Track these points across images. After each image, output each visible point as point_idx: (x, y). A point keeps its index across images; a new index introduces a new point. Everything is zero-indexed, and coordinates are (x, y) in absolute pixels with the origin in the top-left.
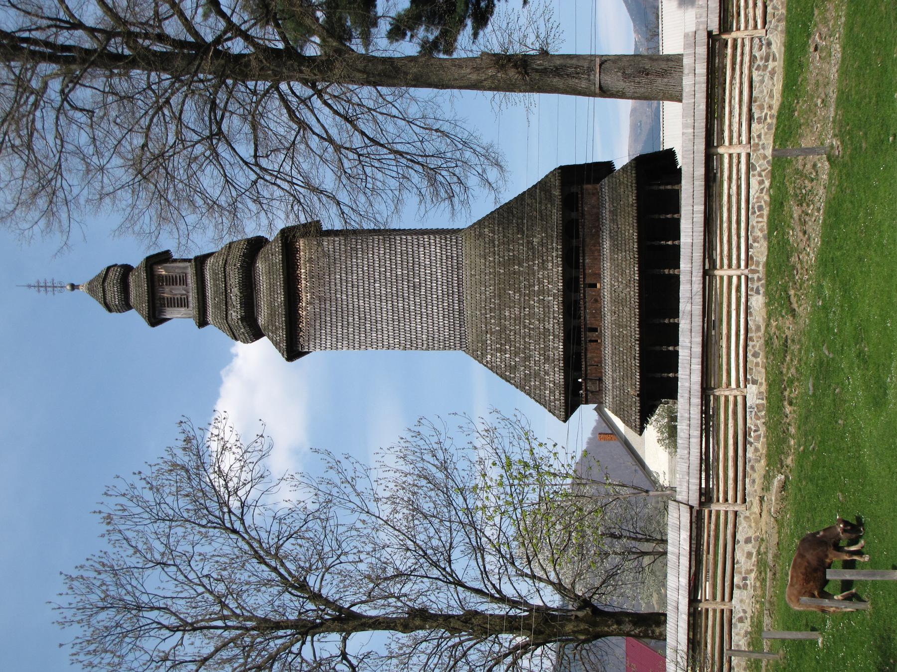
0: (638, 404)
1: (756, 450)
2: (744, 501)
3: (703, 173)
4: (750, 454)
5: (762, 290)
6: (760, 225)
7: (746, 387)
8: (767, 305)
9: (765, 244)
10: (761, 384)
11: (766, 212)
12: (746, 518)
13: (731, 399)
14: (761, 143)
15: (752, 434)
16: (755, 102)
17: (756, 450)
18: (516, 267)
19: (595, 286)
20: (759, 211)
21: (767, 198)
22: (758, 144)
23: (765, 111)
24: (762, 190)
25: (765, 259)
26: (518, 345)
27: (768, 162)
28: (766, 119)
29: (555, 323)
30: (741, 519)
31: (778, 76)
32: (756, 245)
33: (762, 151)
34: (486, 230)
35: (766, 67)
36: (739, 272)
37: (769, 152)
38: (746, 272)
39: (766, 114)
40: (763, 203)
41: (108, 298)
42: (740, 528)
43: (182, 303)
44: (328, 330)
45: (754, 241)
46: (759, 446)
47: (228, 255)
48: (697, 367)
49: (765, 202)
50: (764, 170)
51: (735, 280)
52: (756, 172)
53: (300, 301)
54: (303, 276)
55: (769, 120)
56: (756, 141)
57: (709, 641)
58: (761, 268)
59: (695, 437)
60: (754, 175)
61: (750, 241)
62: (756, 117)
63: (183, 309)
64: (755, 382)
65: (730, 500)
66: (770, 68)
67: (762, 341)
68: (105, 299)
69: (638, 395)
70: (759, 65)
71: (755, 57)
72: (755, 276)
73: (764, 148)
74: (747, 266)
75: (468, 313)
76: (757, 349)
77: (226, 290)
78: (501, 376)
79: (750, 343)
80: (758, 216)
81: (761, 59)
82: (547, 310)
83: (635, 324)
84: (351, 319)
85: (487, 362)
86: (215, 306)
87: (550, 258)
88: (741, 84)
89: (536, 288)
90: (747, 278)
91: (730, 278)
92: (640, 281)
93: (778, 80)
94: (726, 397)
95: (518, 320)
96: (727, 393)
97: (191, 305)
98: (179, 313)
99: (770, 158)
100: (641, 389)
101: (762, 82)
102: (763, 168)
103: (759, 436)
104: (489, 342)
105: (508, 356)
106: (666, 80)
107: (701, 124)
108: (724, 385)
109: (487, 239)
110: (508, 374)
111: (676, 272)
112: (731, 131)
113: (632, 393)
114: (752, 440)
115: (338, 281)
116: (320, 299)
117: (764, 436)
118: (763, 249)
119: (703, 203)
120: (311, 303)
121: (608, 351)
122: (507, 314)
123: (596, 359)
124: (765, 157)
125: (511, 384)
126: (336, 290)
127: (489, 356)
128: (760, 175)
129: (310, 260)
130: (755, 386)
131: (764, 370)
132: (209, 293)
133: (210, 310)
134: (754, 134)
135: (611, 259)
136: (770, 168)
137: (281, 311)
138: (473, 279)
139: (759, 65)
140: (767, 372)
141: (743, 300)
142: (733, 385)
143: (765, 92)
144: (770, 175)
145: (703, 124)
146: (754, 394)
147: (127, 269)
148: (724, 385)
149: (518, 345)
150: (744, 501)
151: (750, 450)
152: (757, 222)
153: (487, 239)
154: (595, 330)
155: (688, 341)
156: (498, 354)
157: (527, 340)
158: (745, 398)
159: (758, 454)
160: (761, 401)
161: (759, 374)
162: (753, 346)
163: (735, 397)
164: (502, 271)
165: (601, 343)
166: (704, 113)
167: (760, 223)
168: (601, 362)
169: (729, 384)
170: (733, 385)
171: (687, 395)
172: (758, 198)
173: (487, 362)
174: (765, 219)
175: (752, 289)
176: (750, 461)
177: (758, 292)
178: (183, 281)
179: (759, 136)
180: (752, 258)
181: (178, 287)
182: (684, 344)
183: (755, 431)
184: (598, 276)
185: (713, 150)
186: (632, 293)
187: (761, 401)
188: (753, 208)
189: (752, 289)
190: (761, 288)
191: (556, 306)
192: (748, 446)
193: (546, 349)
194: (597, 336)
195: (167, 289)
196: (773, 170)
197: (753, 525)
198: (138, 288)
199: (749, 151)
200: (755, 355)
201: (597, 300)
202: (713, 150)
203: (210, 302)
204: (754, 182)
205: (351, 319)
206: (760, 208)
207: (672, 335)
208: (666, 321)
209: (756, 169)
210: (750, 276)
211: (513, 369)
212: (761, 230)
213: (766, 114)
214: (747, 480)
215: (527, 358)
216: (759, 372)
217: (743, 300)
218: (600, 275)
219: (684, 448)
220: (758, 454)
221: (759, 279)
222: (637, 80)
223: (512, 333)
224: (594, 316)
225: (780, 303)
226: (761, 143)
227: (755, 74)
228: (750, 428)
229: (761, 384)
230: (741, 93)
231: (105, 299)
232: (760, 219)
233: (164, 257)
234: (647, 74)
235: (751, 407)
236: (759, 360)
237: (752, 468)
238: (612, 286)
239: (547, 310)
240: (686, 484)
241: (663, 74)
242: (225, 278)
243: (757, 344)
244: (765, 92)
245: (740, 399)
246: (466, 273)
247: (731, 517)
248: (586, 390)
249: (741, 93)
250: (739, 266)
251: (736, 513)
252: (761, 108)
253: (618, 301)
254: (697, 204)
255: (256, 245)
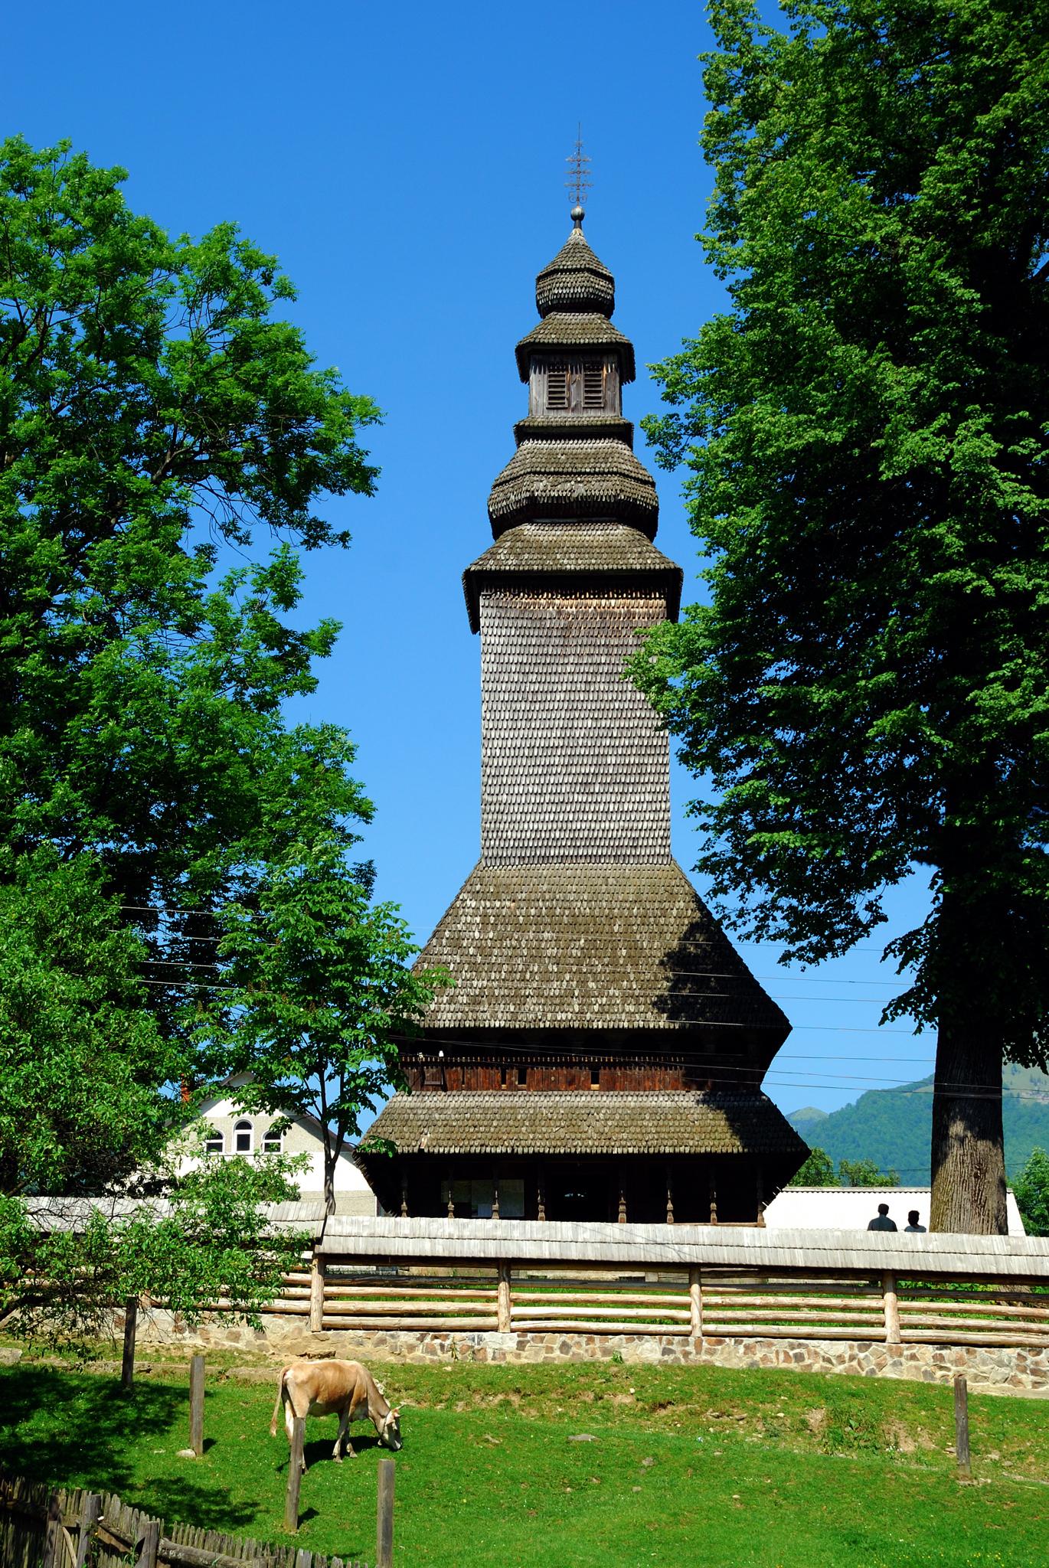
0: (406, 1150)
1: (412, 1348)
2: (326, 1328)
3: (856, 1266)
4: (406, 1337)
5: (669, 1358)
6: (773, 1356)
7: (513, 1331)
8: (649, 1368)
9: (743, 1365)
10: (518, 1356)
11: (792, 1365)
12: (300, 1330)
13: (683, 1314)
14: (903, 1359)
15: (438, 1341)
16: (968, 1352)
17: (412, 1348)
18: (624, 952)
19: (595, 1081)
20: (795, 1355)
21: (816, 1368)
22: (901, 1355)
23: (954, 1368)
24: (829, 1361)
25: (718, 1364)
26: (496, 952)
27: (873, 1371)
28: (941, 1368)
29: (534, 1014)
30: (296, 1322)
31: (1009, 1390)
32: (741, 1349)
33: (890, 1361)
34: (682, 904)
35: (1024, 1371)
36: (696, 1321)
37: (889, 1373)
38: (697, 1333)
39: (948, 1369)
40: (807, 1362)
41: (564, 277)
42: (281, 1321)
43: (556, 400)
44: (515, 640)
45: (747, 1347)
46: (418, 1353)
47: (637, 479)
48: (546, 1252)
49: (810, 1366)
50: (859, 1364)
51: (683, 1314)
52: (856, 1351)
53: (564, 595)
54: (603, 602)
55: (939, 1373)
56: (906, 1353)
57: (728, 1300)
58: (705, 1357)
59: (433, 1246)
60: (851, 1347)
61: (746, 1341)
62: (944, 1352)
63: (545, 400)
64: (521, 1345)
65: (329, 1304)
66: (1023, 1377)
67: (587, 1358)
68: (563, 271)
69: (421, 1151)
70: (1025, 1358)
71: (1038, 1354)
72: (691, 1348)
73: (894, 1364)
74: (706, 1334)
75: (544, 870)
76: (574, 1349)
77: (580, 474)
78: (441, 923)
79: (584, 1338)
80: (786, 1353)
81: (1037, 1363)
82: (558, 1001)
83: (542, 1146)
84: (534, 677)
85: (463, 901)
86: (552, 454)
87: (642, 1008)
88: (991, 1329)
89: (591, 985)
90: (687, 1334)
91: (687, 1306)
92: (609, 1156)
93: (1003, 1390)
94: (495, 1299)
95: (536, 956)
96: (503, 1299)
97: (552, 414)
98: (538, 393)
99: (879, 1375)
100: (431, 1155)
101: (1000, 1364)
102: (864, 1363)
103: (433, 1352)
104: (498, 904)
105: (477, 935)
106: (968, 1206)
107: (838, 1261)
108: (514, 1295)
109: (667, 905)
110: (447, 934)
111: (622, 1216)
112: (796, 1307)
113: (424, 1140)
114: (428, 1340)
115: (596, 659)
116: (568, 628)
117: (432, 1361)
118: (735, 1360)
119: (809, 1265)
120: (559, 613)
121: (488, 1100)
122: (546, 935)
123: (473, 1081)
124: (881, 1366)
125: (431, 940)
126: (580, 655)
127: (474, 904)
128: (852, 1358)
129: (630, 615)
130: (515, 1346)
131: (540, 1360)
132: (572, 445)
133: (544, 445)
134: (917, 1349)
135: (642, 1108)
136: (864, 1374)
137: (549, 565)
138: (600, 881)
139: (1025, 1358)
140: (534, 1367)
141: (653, 1328)
142: (517, 1311)
143: (985, 1368)
144: (851, 1373)
145: (932, 1268)
146: (501, 1344)
147: (604, 306)
148: (514, 1295)
149: (496, 952)
150: (326, 1328)
151: (410, 1337)
152: (777, 1352)
153: (667, 905)
154: (522, 1081)
155: (587, 1236)
156: (478, 919)
157: (505, 967)
158: (495, 1329)
159: (405, 1351)
160: (490, 1356)
161: (534, 1354)
162: (578, 1343)
163: (496, 1314)
164: (616, 928)
165: (500, 1089)
166: (951, 1270)
167: (774, 1356)
168: (469, 1088)
169: (515, 1302)
170: (517, 1311)
171: (499, 1234)
172: (816, 1353)
173: (463, 901)
174: (783, 1365)
175: (670, 1343)
176: (392, 1336)
177: (665, 1352)
178: (593, 401)
179: (913, 1357)
180: (720, 1343)
181: (583, 395)
182: (581, 1231)
183: (442, 1346)
184: (610, 1086)
185: (890, 1284)
186: (587, 1142)
187: (490, 1356)
188: (800, 1345)
189: (670, 1343)
190: (672, 1357)
191: (564, 1017)
192: (418, 1334)
193: (493, 1000)
194: (512, 1083)
195: (579, 377)
196: (860, 1378)
197: (288, 1342)
198: (578, 327)
199: (889, 1339)
200: (565, 1347)
201: (572, 1084)
202: (890, 1284)
203: (557, 445)
204: (841, 1347)
205: (534, 677)
206: (799, 1358)
207: (646, 1212)
208: (622, 1208)
209: (860, 1350)
210: (691, 1339)
211: (456, 943)
212: (765, 1358)
213: (948, 1369)
214: (361, 1333)
215: (474, 967)
216: (537, 1353)
217: (653, 1328)
218: (613, 1089)
219: (412, 1228)
220: (405, 1351)
221: (686, 1354)
222: (968, 1160)
223: (514, 943)
224: (545, 1079)
225: (660, 1392)
226: (903, 1359)
227: (1012, 1352)
228: (447, 1337)
229: (518, 1356)
230: (980, 1329)
231: (563, 271)
232: (782, 1357)
233: (627, 373)
234: (976, 1176)
235: (480, 1339)
236: (558, 1352)
237: (382, 1341)
238: (598, 1109)
239: (558, 1001)
240: (354, 1231)
241: (979, 1203)
242: (598, 473)
243: (583, 1350)
244: (985, 1368)
245: (491, 1321)
246: (609, 868)
247: (302, 1305)
248: (426, 1064)
249: (980, 1329)
250: (705, 1321)
251: (306, 1313)
252: (959, 1362)
253: (574, 1118)
254: (805, 1255)
255: (643, 519)
